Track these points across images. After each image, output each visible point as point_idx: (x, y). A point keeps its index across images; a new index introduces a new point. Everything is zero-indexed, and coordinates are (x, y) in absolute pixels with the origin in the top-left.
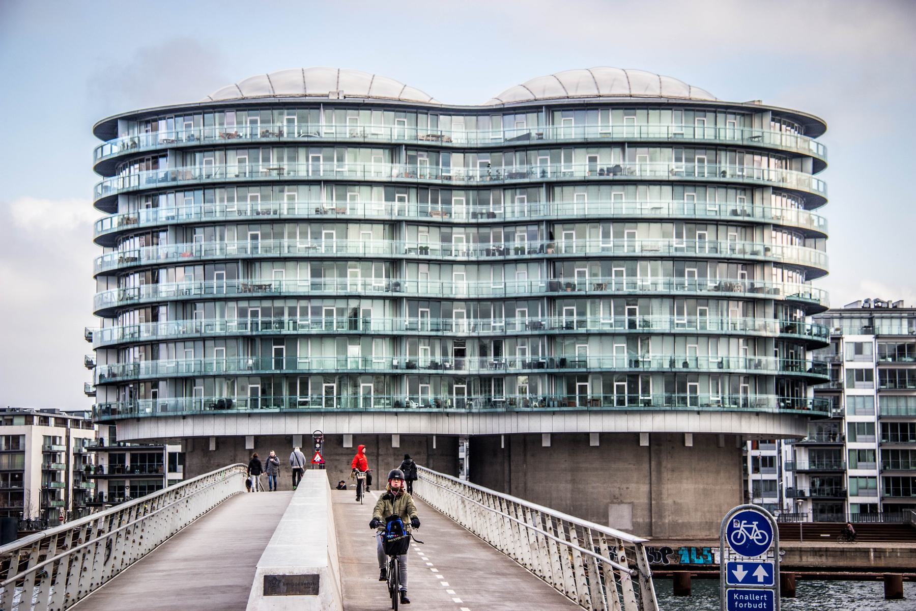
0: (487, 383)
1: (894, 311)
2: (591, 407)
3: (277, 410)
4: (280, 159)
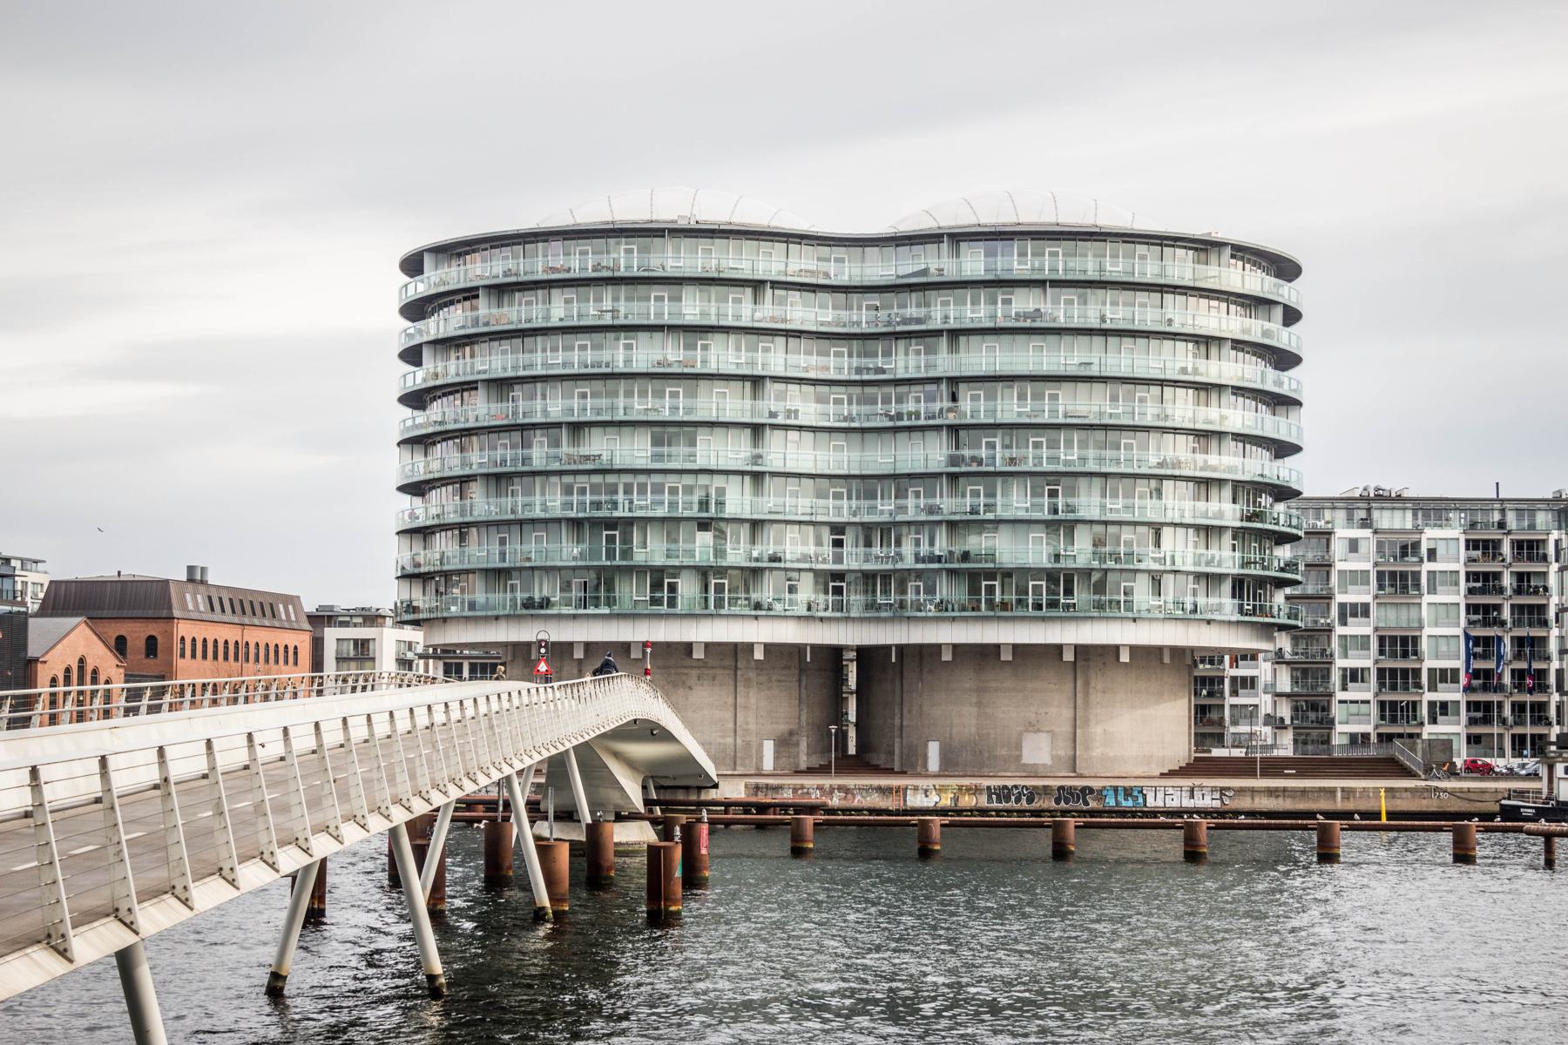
0: (870, 581)
1: (1396, 501)
2: (1002, 612)
3: (606, 611)
4: (616, 299)
